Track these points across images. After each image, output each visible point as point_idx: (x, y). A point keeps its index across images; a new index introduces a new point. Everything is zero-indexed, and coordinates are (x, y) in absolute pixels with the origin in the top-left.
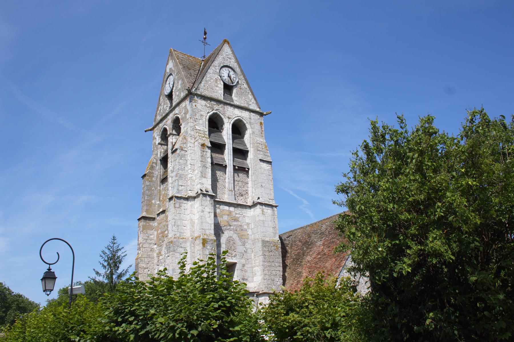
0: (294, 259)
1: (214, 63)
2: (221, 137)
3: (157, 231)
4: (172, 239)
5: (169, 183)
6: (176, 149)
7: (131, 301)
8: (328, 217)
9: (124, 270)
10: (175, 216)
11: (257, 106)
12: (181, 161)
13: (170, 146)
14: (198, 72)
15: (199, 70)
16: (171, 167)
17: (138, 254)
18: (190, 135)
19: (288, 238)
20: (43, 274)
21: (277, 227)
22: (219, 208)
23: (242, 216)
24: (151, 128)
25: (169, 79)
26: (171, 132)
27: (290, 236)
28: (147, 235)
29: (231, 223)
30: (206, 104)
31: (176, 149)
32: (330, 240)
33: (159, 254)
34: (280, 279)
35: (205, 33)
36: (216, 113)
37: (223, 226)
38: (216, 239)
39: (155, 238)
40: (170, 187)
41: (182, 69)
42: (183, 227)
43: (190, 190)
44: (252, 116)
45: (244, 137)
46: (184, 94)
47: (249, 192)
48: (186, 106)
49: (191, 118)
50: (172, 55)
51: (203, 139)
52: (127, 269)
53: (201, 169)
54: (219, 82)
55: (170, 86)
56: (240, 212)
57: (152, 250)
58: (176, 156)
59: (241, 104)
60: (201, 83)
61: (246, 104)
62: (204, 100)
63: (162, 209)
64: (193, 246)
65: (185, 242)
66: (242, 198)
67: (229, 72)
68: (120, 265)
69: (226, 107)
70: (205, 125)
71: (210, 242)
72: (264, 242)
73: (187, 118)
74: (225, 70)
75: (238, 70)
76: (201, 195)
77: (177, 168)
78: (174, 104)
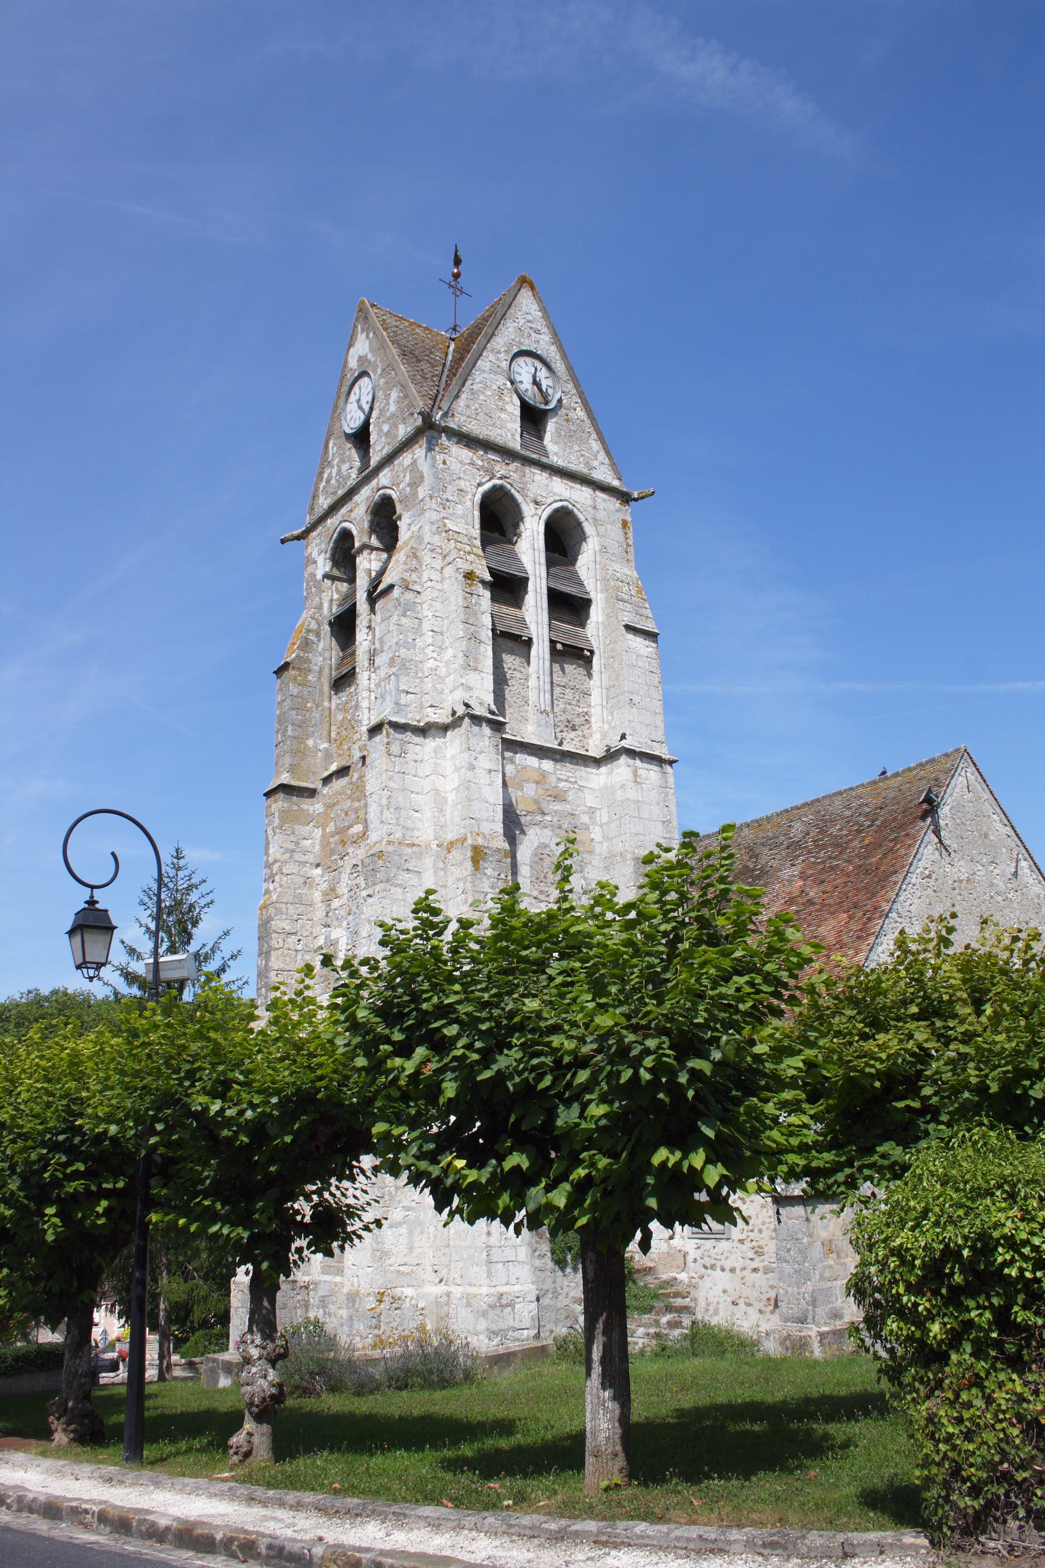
1: (492, 341)
2: (515, 558)
3: (324, 827)
4: (383, 846)
5: (360, 687)
6: (391, 587)
8: (809, 800)
9: (204, 945)
10: (390, 779)
11: (612, 472)
12: (404, 620)
13: (362, 583)
15: (444, 364)
17: (265, 894)
18: (429, 546)
20: (73, 917)
22: (512, 762)
23: (576, 786)
25: (356, 389)
26: (365, 540)
28: (292, 838)
29: (544, 805)
31: (391, 587)
32: (823, 862)
33: (331, 893)
35: (457, 262)
37: (524, 813)
39: (317, 848)
40: (363, 698)
43: (431, 706)
44: (599, 501)
45: (576, 560)
46: (409, 429)
47: (593, 720)
48: (414, 463)
49: (431, 498)
53: (464, 645)
54: (507, 399)
57: (308, 882)
58: (390, 606)
60: (457, 397)
61: (582, 465)
62: (467, 446)
63: (335, 764)
65: (419, 856)
66: (573, 734)
69: (528, 470)
71: (492, 856)
74: (523, 364)
75: (559, 366)
76: (467, 720)
77: (391, 640)
78: (374, 460)
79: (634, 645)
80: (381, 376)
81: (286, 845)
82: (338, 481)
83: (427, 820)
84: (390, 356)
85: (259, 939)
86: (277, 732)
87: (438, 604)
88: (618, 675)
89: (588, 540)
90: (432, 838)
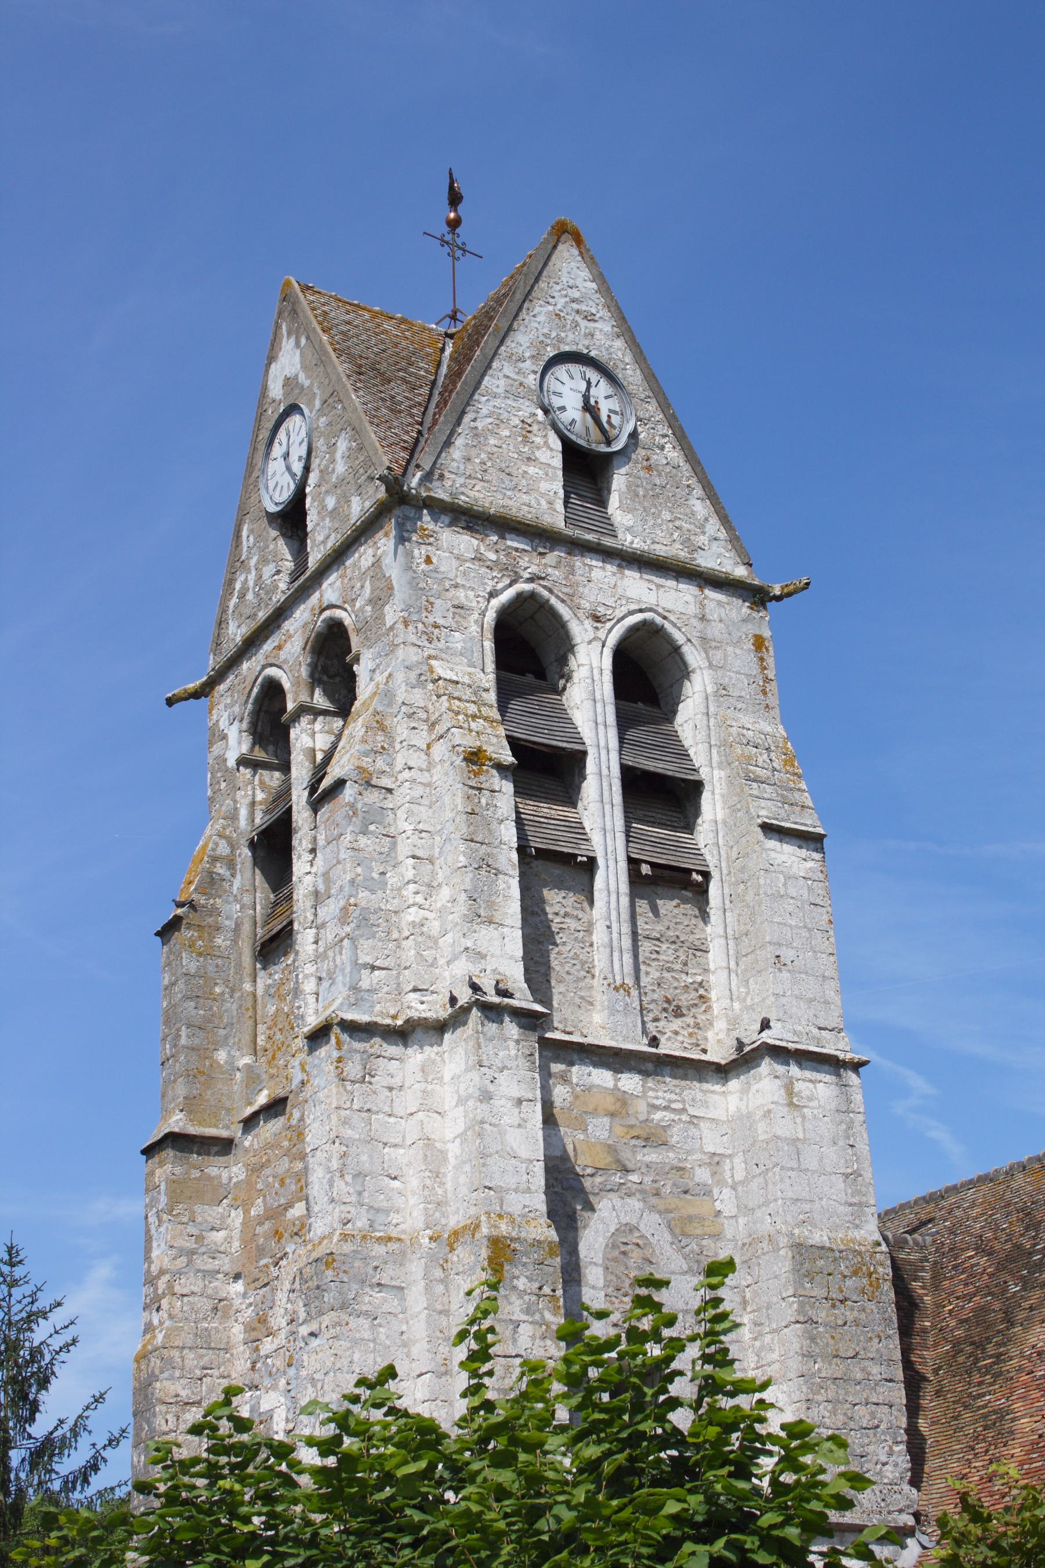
0: (956, 1344)
1: (508, 342)
2: (563, 717)
3: (246, 1207)
4: (333, 1245)
5: (302, 957)
6: (340, 784)
7: (227, 1550)
10: (345, 1122)
11: (733, 554)
12: (363, 841)
13: (300, 772)
14: (431, 395)
15: (434, 383)
16: (308, 879)
17: (145, 1332)
18: (404, 709)
19: (916, 1236)
21: (868, 1174)
22: (565, 1079)
23: (684, 1118)
24: (198, 683)
25: (282, 435)
26: (304, 697)
27: (923, 1224)
28: (191, 1229)
29: (626, 1155)
30: (477, 551)
31: (340, 784)
34: (896, 1449)
35: (455, 199)
36: (533, 595)
37: (589, 1171)
38: (556, 1238)
39: (236, 1244)
40: (306, 976)
41: (348, 376)
42: (387, 1179)
43: (415, 990)
44: (710, 606)
45: (675, 712)
46: (368, 504)
47: (713, 995)
48: (377, 563)
49: (406, 624)
50: (294, 312)
51: (473, 725)
52: (80, 1417)
53: (467, 879)
54: (538, 440)
55: (288, 468)
56: (673, 1097)
57: (220, 1307)
58: (340, 815)
59: (657, 547)
60: (448, 443)
61: (678, 546)
62: (469, 528)
63: (265, 1092)
64: (441, 1281)
65: (400, 1259)
66: (677, 1024)
67: (589, 383)
68: (43, 1396)
69: (578, 562)
70: (477, 655)
71: (526, 1254)
72: (800, 1248)
73: (388, 624)
74: (564, 377)
75: (631, 375)
76: (475, 1013)
77: (343, 876)
78: (315, 558)
79: (779, 858)
80: (321, 412)
81: (180, 1243)
82: (257, 595)
83: (413, 1193)
84: (334, 378)
85: (135, 1415)
86: (164, 1039)
87: (422, 808)
88: (753, 914)
89: (693, 676)
90: (421, 1225)
